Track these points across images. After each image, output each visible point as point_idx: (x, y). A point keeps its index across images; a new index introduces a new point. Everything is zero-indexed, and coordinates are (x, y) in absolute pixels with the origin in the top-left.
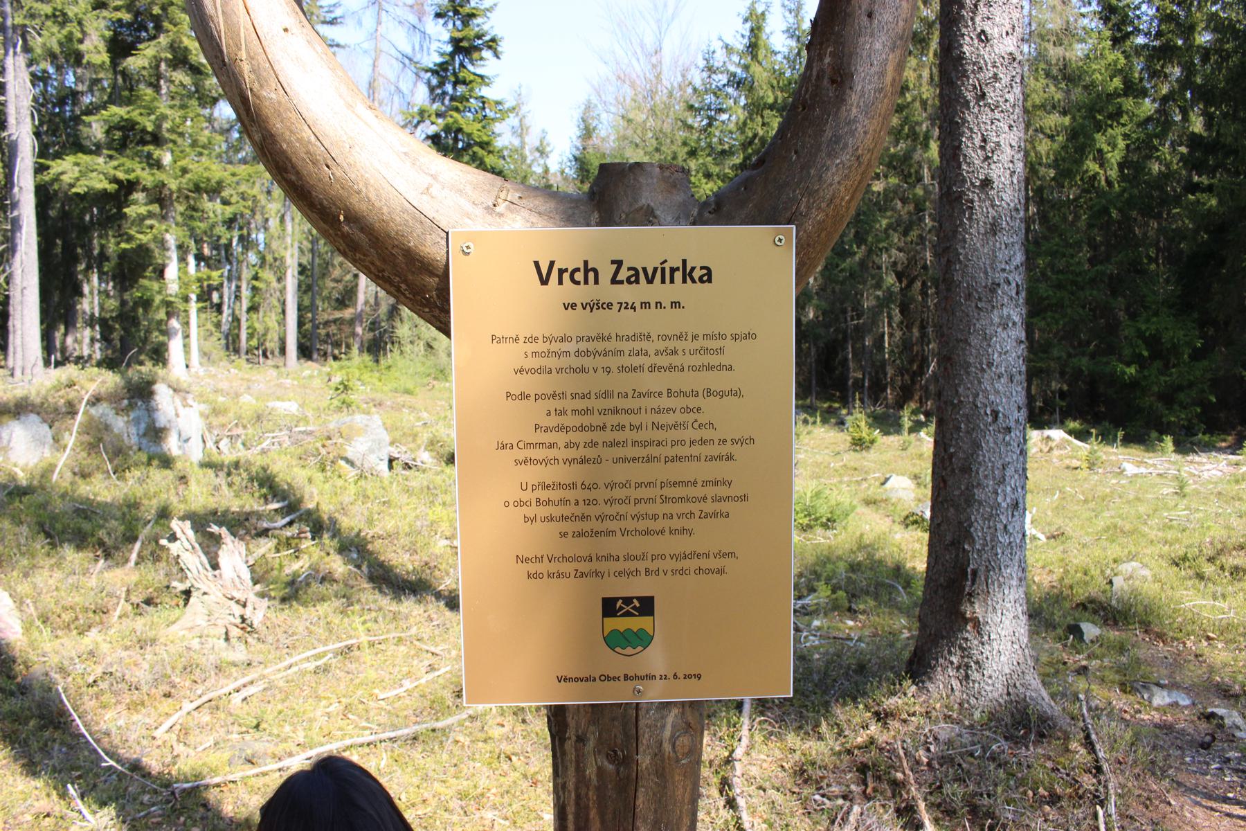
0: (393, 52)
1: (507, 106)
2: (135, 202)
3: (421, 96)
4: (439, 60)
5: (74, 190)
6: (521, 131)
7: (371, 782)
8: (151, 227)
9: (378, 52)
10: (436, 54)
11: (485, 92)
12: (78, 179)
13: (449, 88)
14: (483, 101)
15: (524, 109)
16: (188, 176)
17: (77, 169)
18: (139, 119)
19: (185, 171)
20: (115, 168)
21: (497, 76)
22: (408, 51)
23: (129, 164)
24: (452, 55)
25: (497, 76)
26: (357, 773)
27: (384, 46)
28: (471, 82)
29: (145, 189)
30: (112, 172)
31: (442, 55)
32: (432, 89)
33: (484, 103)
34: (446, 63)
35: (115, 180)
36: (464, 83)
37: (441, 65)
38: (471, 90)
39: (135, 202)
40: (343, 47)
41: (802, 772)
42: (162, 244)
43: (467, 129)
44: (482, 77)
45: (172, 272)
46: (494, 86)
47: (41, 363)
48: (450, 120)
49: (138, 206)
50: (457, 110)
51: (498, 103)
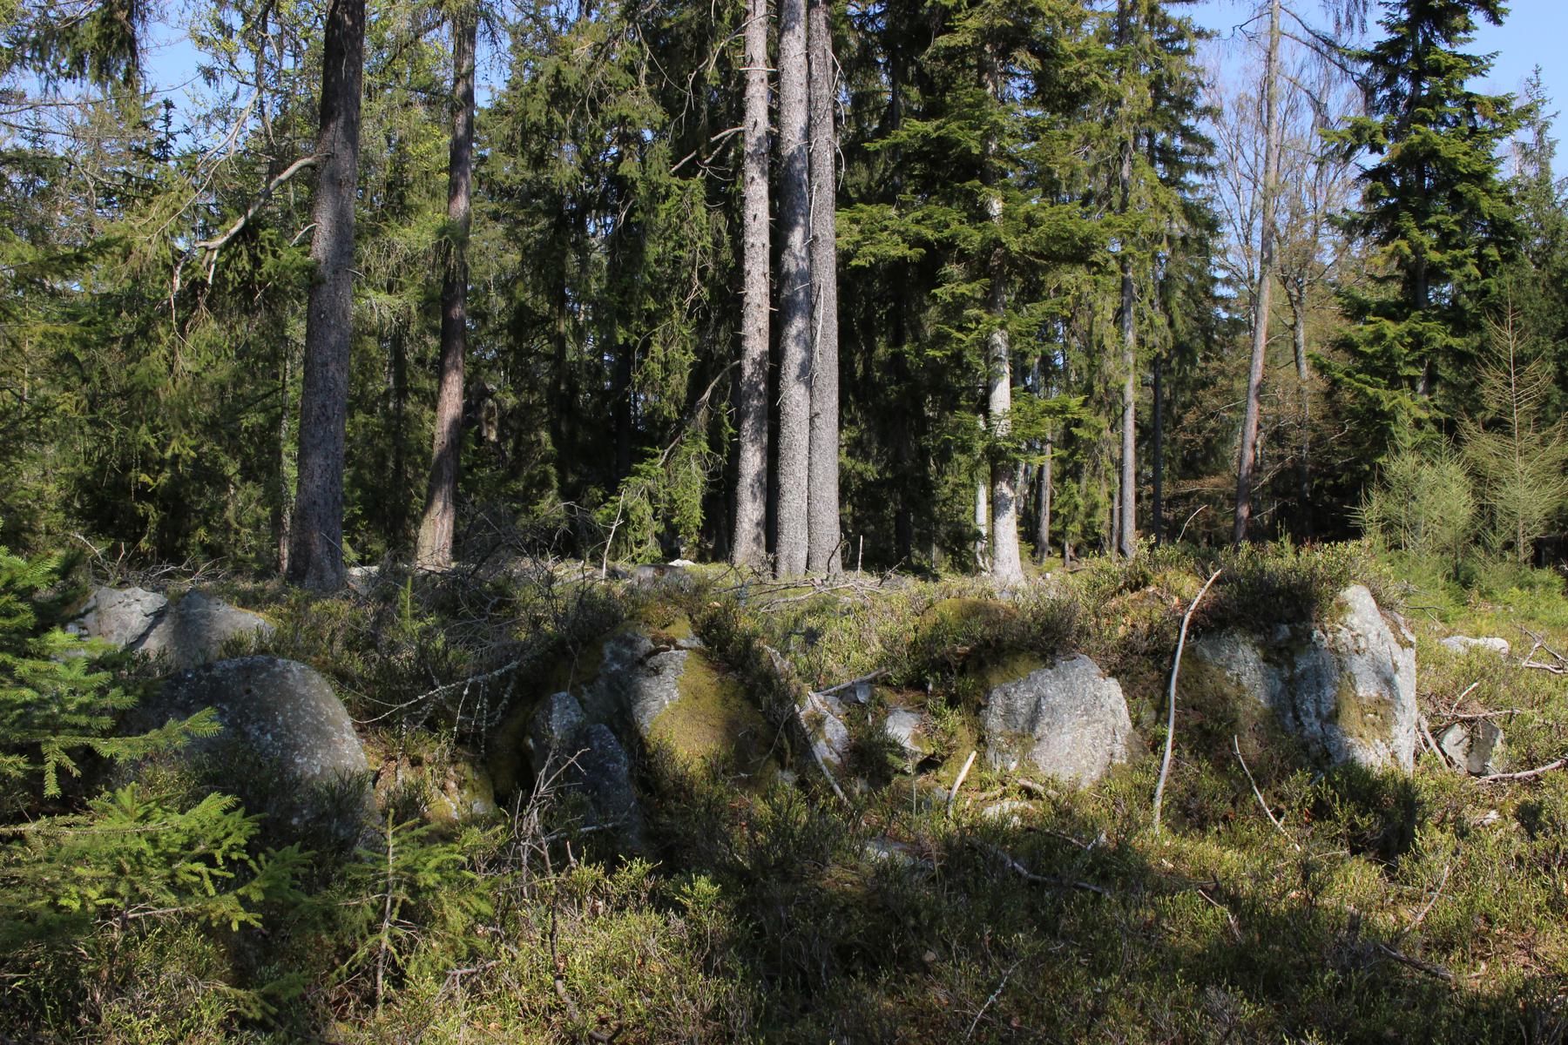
0: (1301, 33)
1: (1515, 106)
2: (948, 279)
3: (1344, 101)
4: (1385, 37)
5: (854, 263)
6: (1539, 153)
7: (724, 522)
8: (978, 320)
9: (1275, 34)
10: (1381, 28)
11: (1472, 85)
12: (858, 244)
13: (1406, 86)
14: (1469, 101)
15: (1546, 111)
16: (1037, 232)
17: (856, 228)
18: (959, 135)
19: (1030, 221)
20: (918, 222)
21: (1494, 55)
22: (1328, 28)
23: (939, 211)
24: (1412, 24)
25: (1494, 55)
26: (724, 522)
27: (1286, 23)
28: (1450, 68)
29: (963, 257)
30: (914, 228)
31: (1391, 28)
32: (1368, 89)
33: (1469, 105)
34: (1402, 40)
35: (918, 241)
36: (1437, 71)
37: (1391, 45)
38: (1449, 84)
39: (948, 279)
40: (1209, 37)
41: (1187, 813)
42: (985, 346)
43: (1445, 152)
44: (1467, 58)
45: (1001, 397)
46: (1492, 73)
47: (837, 562)
48: (1416, 138)
49: (956, 283)
50: (1424, 120)
51: (1499, 103)
